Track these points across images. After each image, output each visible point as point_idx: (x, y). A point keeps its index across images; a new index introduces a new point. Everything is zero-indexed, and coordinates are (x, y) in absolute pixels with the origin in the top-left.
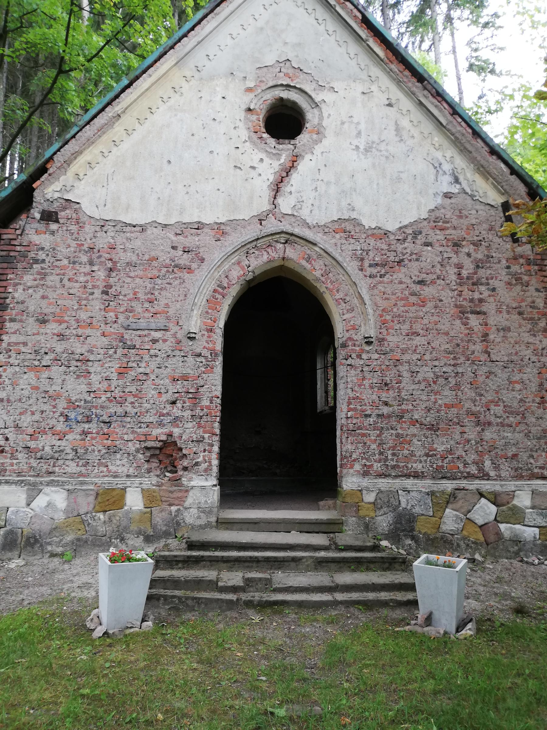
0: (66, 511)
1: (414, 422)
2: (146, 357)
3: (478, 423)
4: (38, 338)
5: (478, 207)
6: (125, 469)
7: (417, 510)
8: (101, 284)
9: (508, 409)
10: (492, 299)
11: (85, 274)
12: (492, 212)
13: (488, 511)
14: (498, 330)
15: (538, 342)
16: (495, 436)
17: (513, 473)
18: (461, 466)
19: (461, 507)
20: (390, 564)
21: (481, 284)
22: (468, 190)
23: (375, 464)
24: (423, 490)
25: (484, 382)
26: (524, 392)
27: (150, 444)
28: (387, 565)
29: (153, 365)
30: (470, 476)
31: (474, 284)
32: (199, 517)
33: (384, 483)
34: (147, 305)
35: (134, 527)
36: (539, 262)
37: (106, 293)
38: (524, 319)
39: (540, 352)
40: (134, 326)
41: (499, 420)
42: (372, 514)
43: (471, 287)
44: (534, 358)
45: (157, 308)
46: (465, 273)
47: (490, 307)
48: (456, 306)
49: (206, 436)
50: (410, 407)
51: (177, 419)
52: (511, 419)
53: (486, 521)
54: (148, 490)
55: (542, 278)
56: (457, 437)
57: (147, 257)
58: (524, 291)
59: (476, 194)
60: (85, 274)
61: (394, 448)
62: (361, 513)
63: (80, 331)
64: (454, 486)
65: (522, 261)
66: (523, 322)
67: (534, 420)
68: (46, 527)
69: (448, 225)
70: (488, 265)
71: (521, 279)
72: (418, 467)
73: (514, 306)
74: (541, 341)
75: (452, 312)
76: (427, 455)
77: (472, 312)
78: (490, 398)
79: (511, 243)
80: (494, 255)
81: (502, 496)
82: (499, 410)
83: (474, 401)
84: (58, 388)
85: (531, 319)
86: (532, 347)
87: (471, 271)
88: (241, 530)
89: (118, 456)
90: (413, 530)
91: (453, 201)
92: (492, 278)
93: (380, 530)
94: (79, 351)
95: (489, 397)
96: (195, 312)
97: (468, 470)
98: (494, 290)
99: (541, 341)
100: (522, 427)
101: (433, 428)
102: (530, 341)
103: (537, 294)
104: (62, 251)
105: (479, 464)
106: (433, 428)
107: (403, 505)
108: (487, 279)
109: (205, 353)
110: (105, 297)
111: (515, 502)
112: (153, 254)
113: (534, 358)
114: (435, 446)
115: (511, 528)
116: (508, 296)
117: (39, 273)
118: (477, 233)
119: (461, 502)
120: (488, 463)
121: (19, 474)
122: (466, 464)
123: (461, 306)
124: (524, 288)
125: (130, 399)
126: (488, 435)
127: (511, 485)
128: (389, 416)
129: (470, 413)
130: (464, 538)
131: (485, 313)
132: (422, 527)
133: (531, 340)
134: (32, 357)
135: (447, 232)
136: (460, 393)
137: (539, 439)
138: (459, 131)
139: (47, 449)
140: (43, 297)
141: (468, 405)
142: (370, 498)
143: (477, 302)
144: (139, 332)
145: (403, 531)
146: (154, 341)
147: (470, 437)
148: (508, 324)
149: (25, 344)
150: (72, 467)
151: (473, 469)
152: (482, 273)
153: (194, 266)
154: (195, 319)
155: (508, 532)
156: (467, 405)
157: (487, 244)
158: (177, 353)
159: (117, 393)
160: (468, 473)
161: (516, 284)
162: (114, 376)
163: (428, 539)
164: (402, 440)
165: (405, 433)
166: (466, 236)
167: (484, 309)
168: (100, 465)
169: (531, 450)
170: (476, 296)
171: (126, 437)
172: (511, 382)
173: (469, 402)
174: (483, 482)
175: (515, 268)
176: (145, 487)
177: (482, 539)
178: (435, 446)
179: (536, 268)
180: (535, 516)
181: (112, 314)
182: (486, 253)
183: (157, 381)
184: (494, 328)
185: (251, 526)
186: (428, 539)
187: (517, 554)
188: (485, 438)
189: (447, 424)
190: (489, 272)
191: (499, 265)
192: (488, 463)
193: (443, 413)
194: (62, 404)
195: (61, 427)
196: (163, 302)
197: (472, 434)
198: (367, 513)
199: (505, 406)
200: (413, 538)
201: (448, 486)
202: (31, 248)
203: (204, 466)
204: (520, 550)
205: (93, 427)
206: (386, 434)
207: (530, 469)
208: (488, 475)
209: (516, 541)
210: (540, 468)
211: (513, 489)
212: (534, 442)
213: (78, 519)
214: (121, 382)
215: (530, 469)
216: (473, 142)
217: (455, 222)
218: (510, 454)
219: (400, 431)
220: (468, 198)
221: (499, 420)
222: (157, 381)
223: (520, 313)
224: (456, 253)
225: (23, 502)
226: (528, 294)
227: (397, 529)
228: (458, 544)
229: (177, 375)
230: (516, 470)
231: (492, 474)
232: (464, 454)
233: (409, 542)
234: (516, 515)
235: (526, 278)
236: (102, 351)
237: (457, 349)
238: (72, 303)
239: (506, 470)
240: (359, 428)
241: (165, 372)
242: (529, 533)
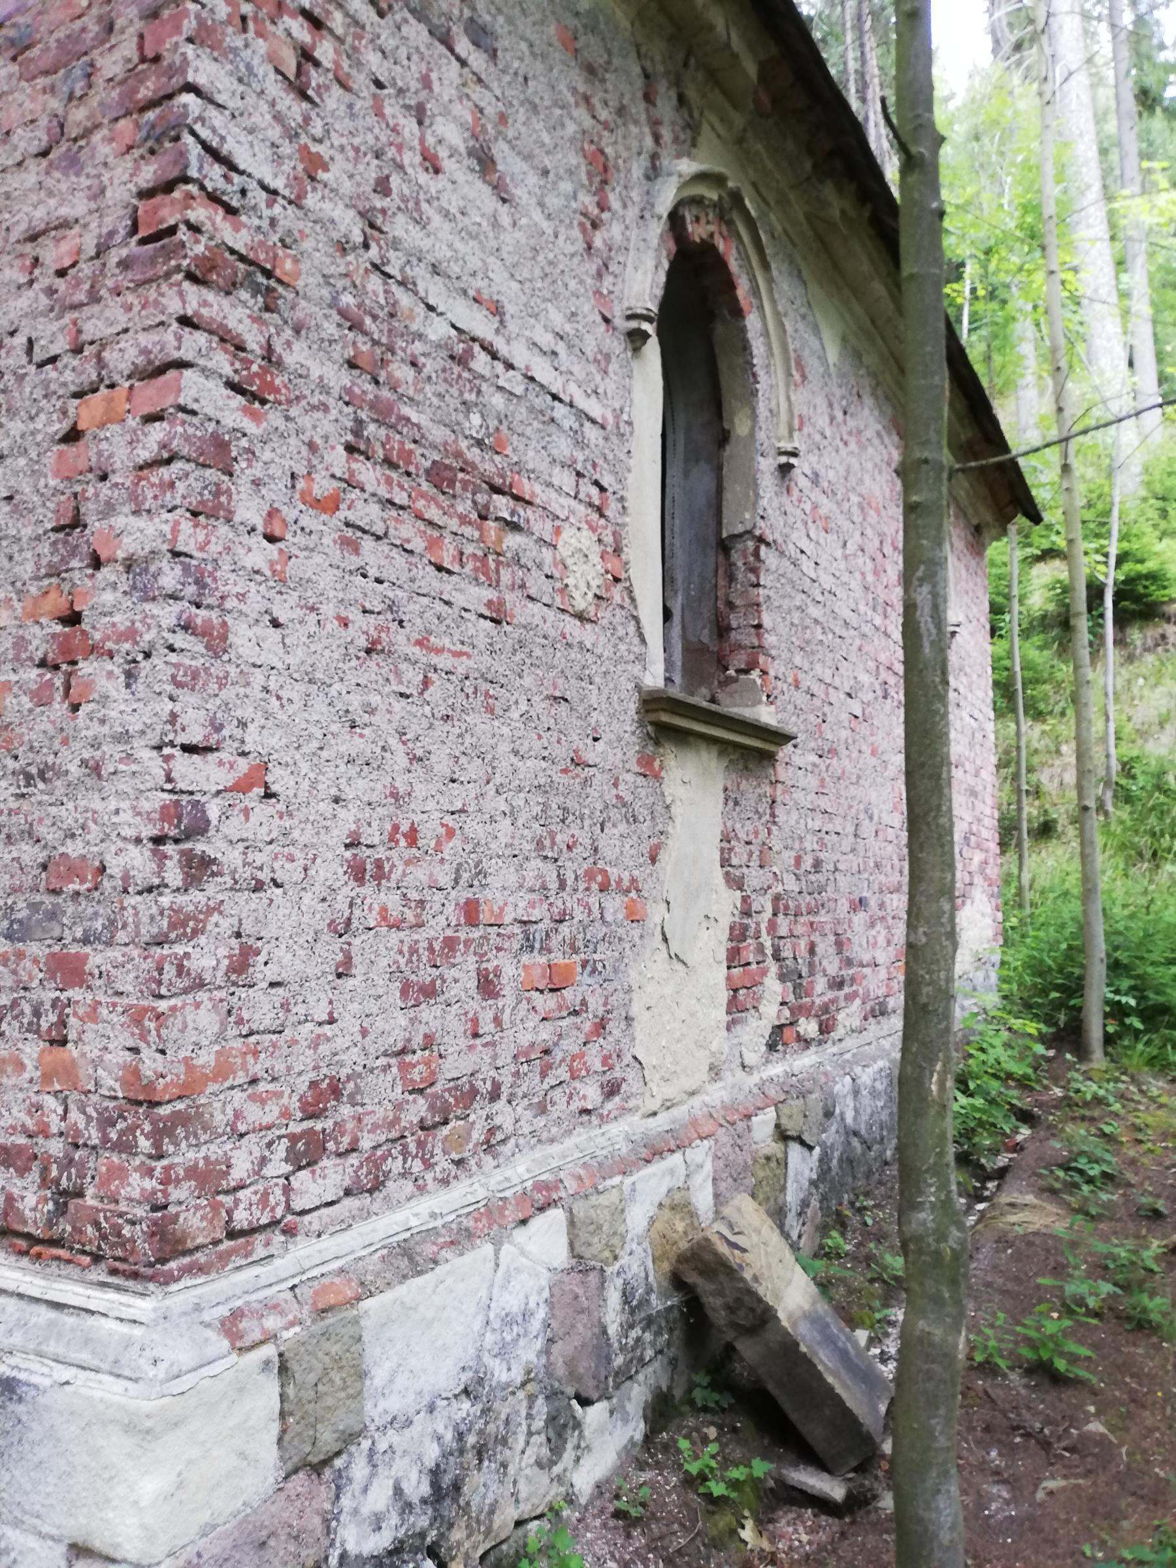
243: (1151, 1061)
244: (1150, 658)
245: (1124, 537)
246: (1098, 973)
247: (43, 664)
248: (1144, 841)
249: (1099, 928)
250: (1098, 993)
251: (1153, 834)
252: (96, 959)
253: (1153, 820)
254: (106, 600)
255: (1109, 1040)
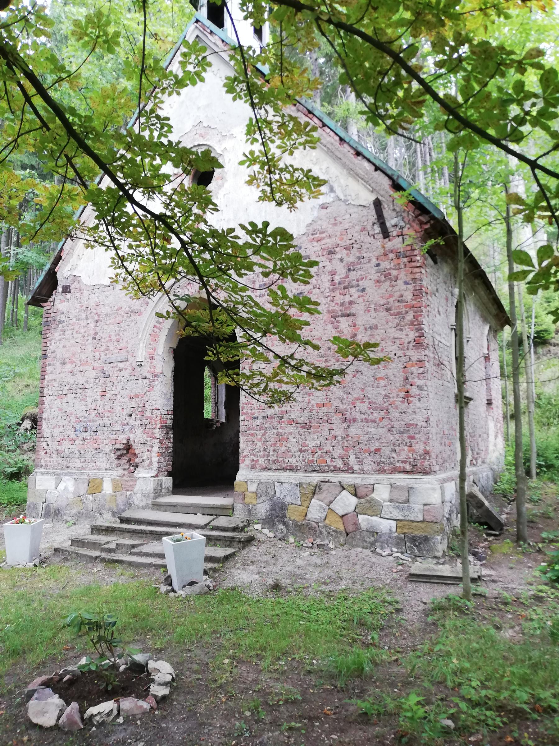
0: (74, 493)
1: (292, 421)
2: (116, 383)
3: (345, 420)
4: (61, 375)
5: (351, 211)
6: (104, 464)
7: (288, 499)
8: (92, 332)
9: (373, 405)
10: (361, 299)
11: (85, 327)
12: (365, 211)
13: (347, 503)
14: (366, 329)
15: (404, 336)
16: (359, 432)
17: (375, 467)
18: (329, 460)
19: (325, 498)
20: (231, 542)
21: (352, 287)
22: (342, 197)
23: (260, 460)
24: (294, 482)
25: (351, 381)
26: (389, 387)
27: (118, 446)
28: (228, 543)
29: (119, 388)
30: (336, 470)
31: (345, 288)
32: (142, 501)
33: (265, 476)
34: (116, 344)
35: (107, 507)
36: (408, 253)
37: (94, 338)
38: (391, 315)
39: (406, 345)
40: (108, 361)
41: (363, 417)
42: (254, 502)
43: (342, 291)
44: (399, 353)
45: (122, 345)
46: (337, 279)
47: (359, 308)
48: (329, 312)
49: (149, 439)
50: (289, 408)
51: (132, 427)
52: (375, 415)
53: (346, 512)
54: (472, 496)
55: (410, 270)
56: (326, 433)
57: (116, 308)
58: (393, 286)
59: (349, 198)
60: (85, 327)
61: (274, 445)
62: (247, 500)
63: (82, 368)
64: (322, 479)
65: (391, 256)
66: (390, 318)
67: (397, 415)
68: (64, 504)
69: (324, 235)
70: (359, 266)
71: (390, 274)
72: (293, 461)
73: (382, 303)
74: (407, 335)
75: (325, 318)
76: (301, 451)
77: (343, 315)
78: (355, 396)
79: (382, 240)
80: (365, 255)
81: (361, 488)
82: (364, 407)
83: (342, 400)
84: (71, 409)
85: (399, 313)
86: (398, 342)
87: (343, 276)
88: (166, 511)
89: (101, 455)
90: (284, 516)
91: (329, 210)
92: (362, 279)
93: (259, 515)
94: (81, 382)
95: (355, 394)
96: (141, 345)
97: (334, 464)
98: (363, 290)
99: (407, 335)
100: (385, 422)
101: (307, 426)
102: (396, 336)
103: (405, 287)
104: (74, 312)
105: (345, 459)
106: (307, 426)
107: (278, 495)
108: (358, 281)
109: (149, 376)
110: (94, 341)
111: (374, 495)
112: (119, 305)
113: (399, 353)
114: (307, 442)
115: (368, 520)
116: (375, 294)
117: (62, 330)
118: (350, 236)
119: (325, 493)
120: (352, 458)
121: (53, 468)
122: (333, 459)
123: (333, 311)
124: (393, 283)
125: (107, 414)
126: (353, 431)
127: (371, 479)
128: (272, 418)
129: (337, 411)
130: (326, 527)
131: (354, 315)
132: (292, 514)
133: (398, 334)
134: (58, 388)
135: (323, 242)
136: (329, 393)
137: (402, 433)
138: (328, 142)
139: (66, 451)
140: (64, 347)
141: (336, 403)
142: (252, 488)
143: (347, 305)
144: (112, 365)
145: (277, 517)
146: (120, 370)
147: (337, 433)
148: (375, 322)
149: (55, 380)
150: (78, 463)
151: (339, 463)
152: (353, 275)
153: (142, 309)
154: (141, 350)
155: (365, 523)
156: (335, 404)
157: (358, 246)
158: (133, 378)
159: (100, 411)
160: (335, 467)
161: (385, 281)
162: (99, 398)
163: (296, 525)
164: (281, 438)
165: (283, 432)
166: (339, 242)
167: (353, 311)
168: (92, 461)
169: (394, 444)
170: (347, 299)
171: (105, 442)
172: (376, 379)
173: (337, 400)
174: (347, 475)
175: (385, 265)
176: (113, 477)
177: (342, 528)
178: (307, 442)
179: (405, 260)
180: (391, 509)
181: (97, 353)
182: (358, 254)
183: (122, 400)
184: (362, 328)
185: (172, 508)
186: (296, 525)
187: (373, 544)
188: (351, 434)
189: (318, 422)
190: (359, 273)
191: (369, 265)
192: (352, 458)
193: (314, 412)
194: (73, 420)
195: (72, 436)
196: (125, 340)
197: (339, 431)
198: (251, 501)
199: (370, 403)
200: (284, 523)
201: (316, 478)
202: (59, 313)
203: (148, 462)
204: (376, 541)
205: (88, 435)
206: (269, 433)
207: (392, 463)
208: (352, 468)
209: (373, 532)
210: (402, 462)
211: (372, 482)
212: (397, 436)
213: (79, 499)
214: (102, 402)
215: (392, 463)
216: (341, 148)
217: (330, 231)
218: (372, 449)
219: (280, 430)
220: (342, 203)
221: (363, 417)
222: (122, 400)
223: (388, 310)
224: (331, 260)
225: (54, 487)
226: (396, 289)
227: (272, 515)
228: (321, 532)
229: (132, 395)
230: (379, 464)
231: (356, 467)
232: (331, 449)
233: (281, 526)
234: (373, 508)
235: (394, 273)
236: (92, 381)
237: (328, 352)
238: (77, 349)
239: (369, 463)
240: (250, 429)
241: (125, 393)
242: (385, 526)
243: (549, 479)
244: (545, 358)
245: (536, 317)
246: (534, 456)
247: (96, 334)
248: (545, 420)
249: (534, 445)
250: (534, 462)
251: (547, 418)
252: (417, 436)
253: (547, 414)
254: (414, 391)
255: (538, 474)
